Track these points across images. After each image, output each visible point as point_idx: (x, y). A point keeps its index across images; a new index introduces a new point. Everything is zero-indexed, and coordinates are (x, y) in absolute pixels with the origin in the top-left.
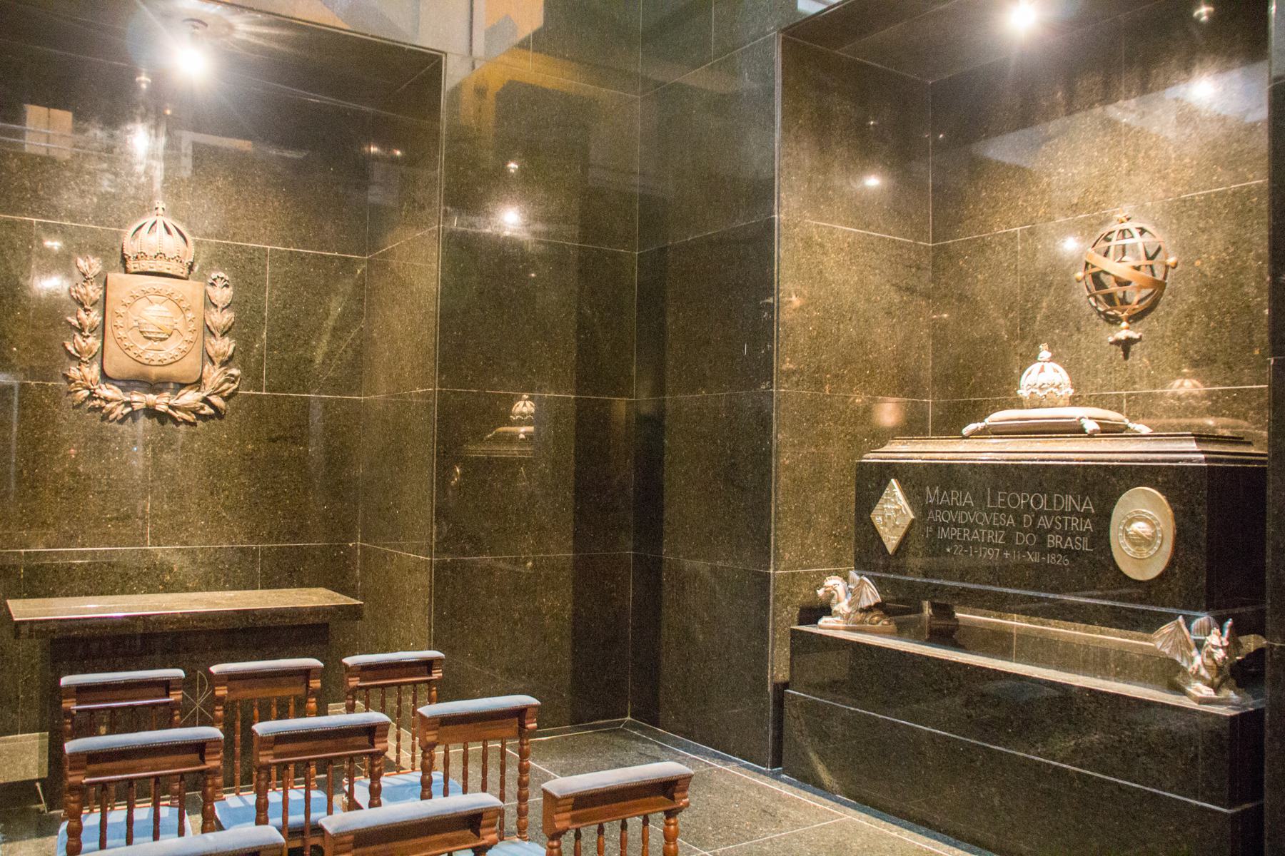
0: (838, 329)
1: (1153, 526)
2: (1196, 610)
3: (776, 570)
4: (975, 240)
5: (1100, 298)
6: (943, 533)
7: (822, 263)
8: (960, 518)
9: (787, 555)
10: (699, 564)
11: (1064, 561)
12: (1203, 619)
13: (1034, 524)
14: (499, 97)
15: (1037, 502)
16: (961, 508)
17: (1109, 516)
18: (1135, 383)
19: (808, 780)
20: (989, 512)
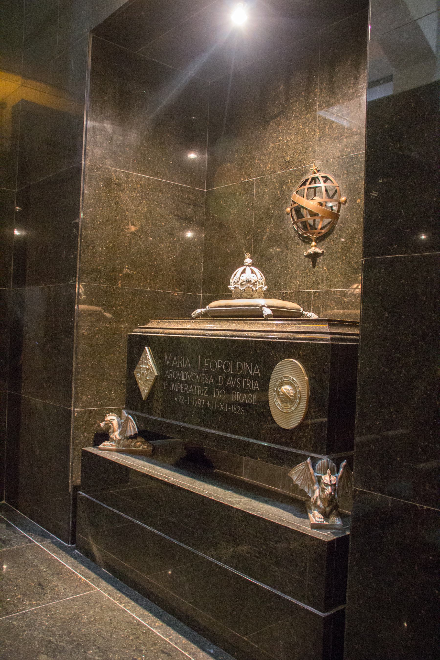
0: (130, 243)
1: (295, 388)
2: (320, 454)
3: (75, 407)
4: (230, 187)
5: (300, 225)
6: (173, 387)
7: (119, 197)
8: (183, 376)
9: (85, 398)
10: (38, 400)
11: (241, 412)
12: (324, 460)
13: (225, 383)
14: (13, 108)
15: (227, 368)
16: (184, 370)
17: (269, 380)
18: (318, 284)
19: (87, 558)
20: (200, 372)
